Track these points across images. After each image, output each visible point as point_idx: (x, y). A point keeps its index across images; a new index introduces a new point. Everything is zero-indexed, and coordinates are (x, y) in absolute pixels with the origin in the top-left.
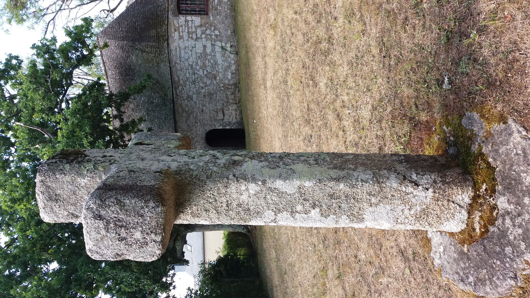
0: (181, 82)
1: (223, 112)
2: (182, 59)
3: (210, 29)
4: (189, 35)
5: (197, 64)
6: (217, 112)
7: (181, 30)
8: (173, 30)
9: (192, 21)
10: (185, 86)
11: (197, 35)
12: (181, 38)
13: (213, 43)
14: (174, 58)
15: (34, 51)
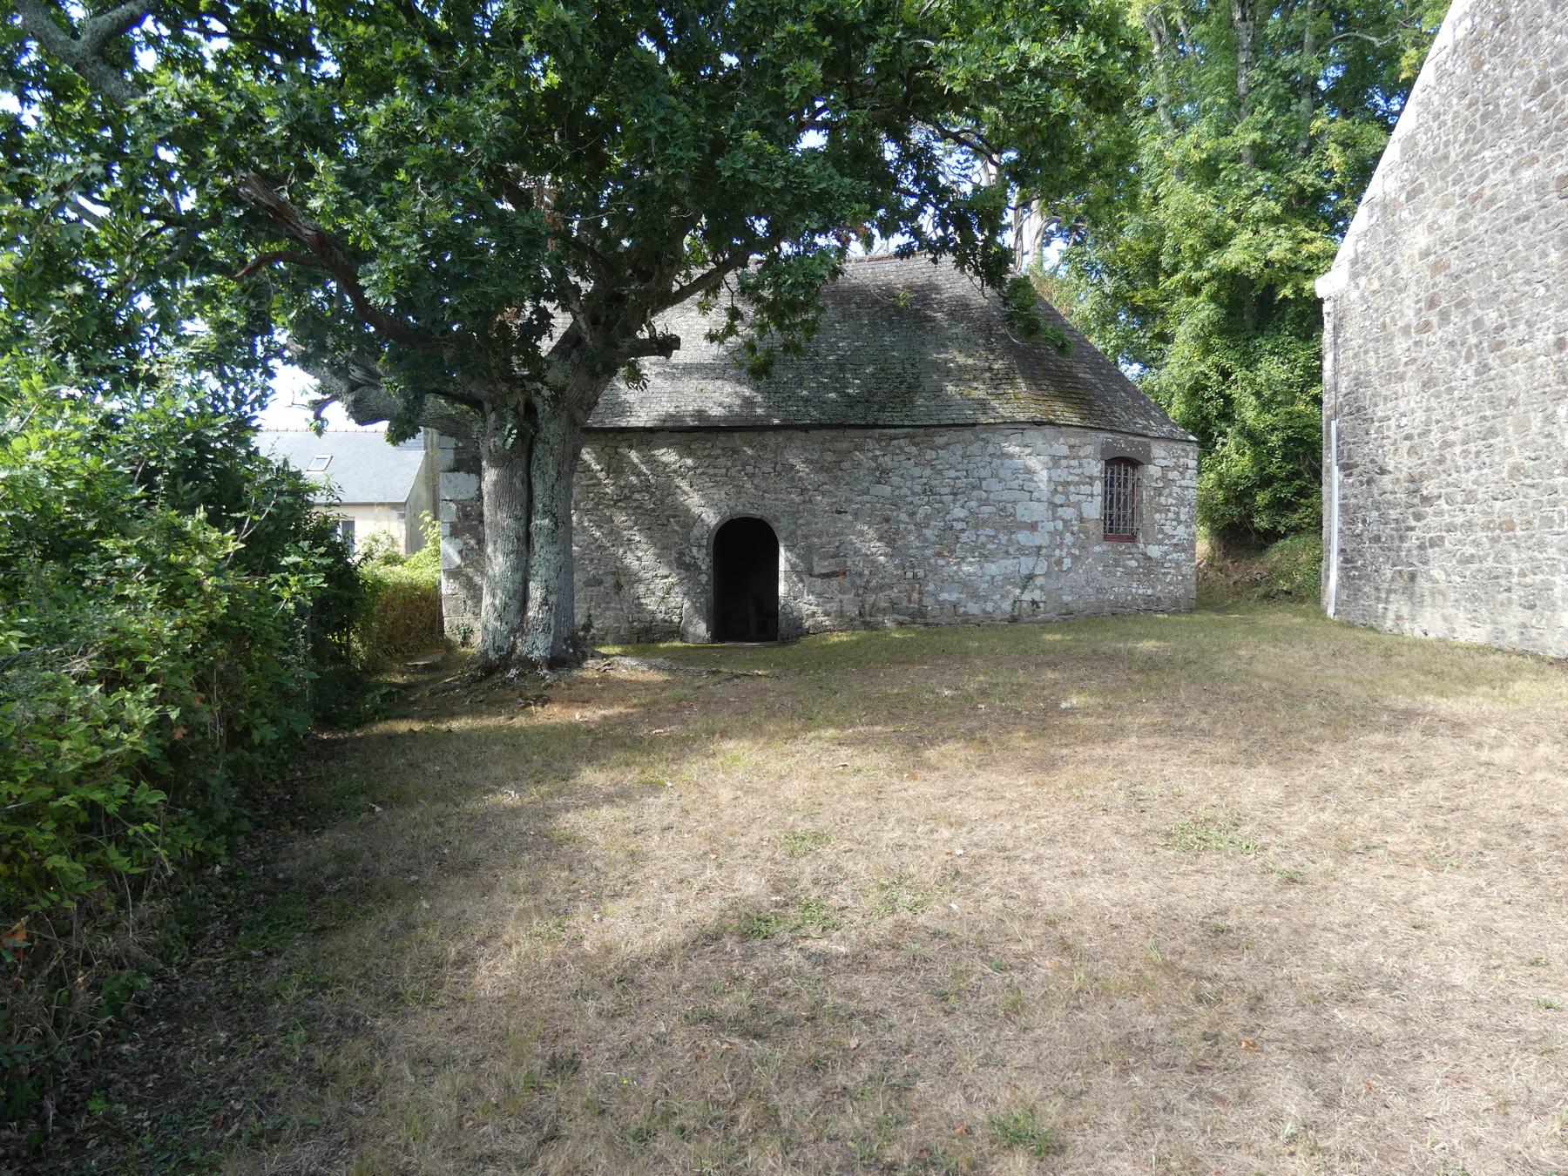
0: (930, 454)
2: (997, 462)
5: (984, 502)
8: (1072, 441)
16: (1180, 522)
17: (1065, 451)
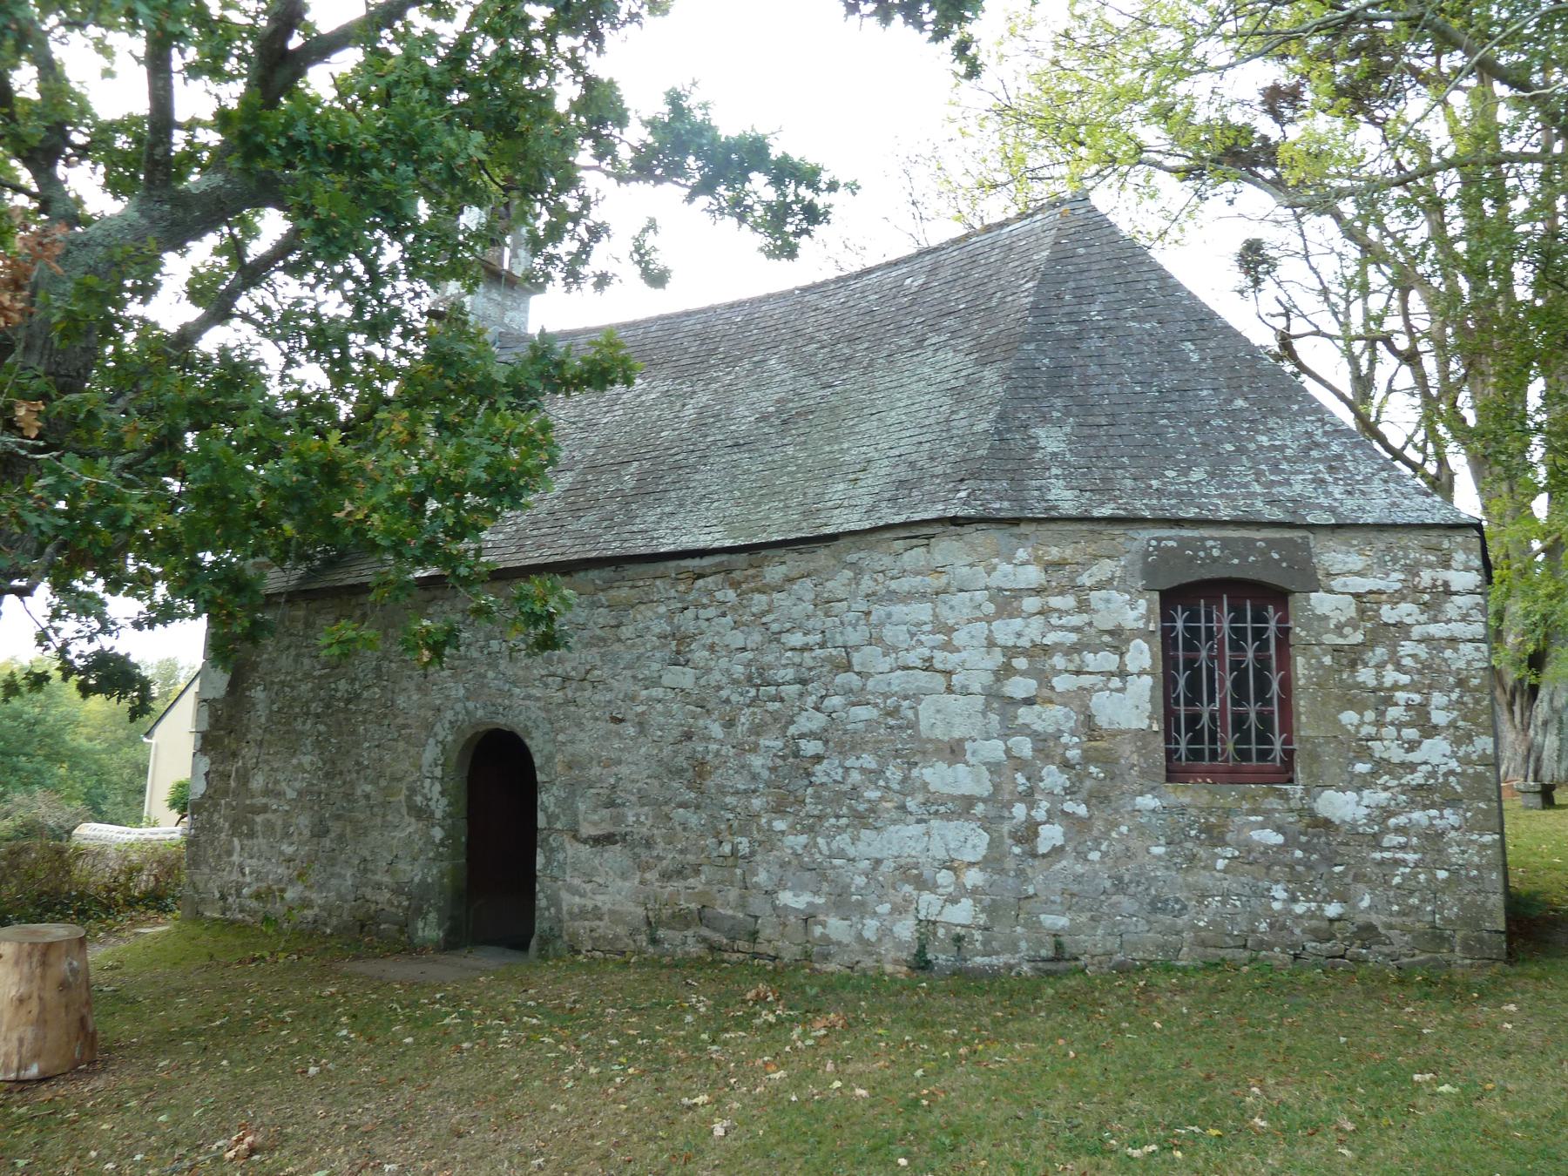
0: (760, 601)
1: (609, 839)
2: (879, 611)
3: (1069, 791)
4: (1025, 652)
5: (856, 698)
6: (611, 804)
7: (1056, 602)
8: (1054, 553)
9: (1122, 674)
10: (736, 625)
11: (1029, 702)
12: (1006, 602)
13: (979, 809)
14: (887, 561)
15: (663, 110)
16: (1429, 731)
17: (1033, 575)
